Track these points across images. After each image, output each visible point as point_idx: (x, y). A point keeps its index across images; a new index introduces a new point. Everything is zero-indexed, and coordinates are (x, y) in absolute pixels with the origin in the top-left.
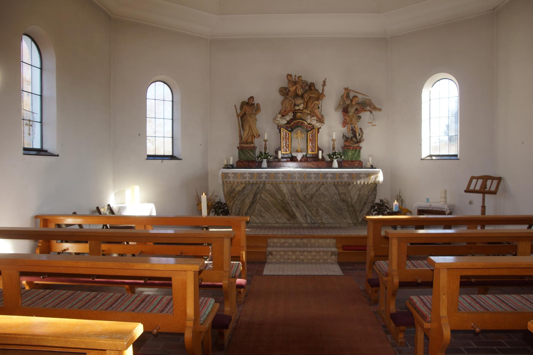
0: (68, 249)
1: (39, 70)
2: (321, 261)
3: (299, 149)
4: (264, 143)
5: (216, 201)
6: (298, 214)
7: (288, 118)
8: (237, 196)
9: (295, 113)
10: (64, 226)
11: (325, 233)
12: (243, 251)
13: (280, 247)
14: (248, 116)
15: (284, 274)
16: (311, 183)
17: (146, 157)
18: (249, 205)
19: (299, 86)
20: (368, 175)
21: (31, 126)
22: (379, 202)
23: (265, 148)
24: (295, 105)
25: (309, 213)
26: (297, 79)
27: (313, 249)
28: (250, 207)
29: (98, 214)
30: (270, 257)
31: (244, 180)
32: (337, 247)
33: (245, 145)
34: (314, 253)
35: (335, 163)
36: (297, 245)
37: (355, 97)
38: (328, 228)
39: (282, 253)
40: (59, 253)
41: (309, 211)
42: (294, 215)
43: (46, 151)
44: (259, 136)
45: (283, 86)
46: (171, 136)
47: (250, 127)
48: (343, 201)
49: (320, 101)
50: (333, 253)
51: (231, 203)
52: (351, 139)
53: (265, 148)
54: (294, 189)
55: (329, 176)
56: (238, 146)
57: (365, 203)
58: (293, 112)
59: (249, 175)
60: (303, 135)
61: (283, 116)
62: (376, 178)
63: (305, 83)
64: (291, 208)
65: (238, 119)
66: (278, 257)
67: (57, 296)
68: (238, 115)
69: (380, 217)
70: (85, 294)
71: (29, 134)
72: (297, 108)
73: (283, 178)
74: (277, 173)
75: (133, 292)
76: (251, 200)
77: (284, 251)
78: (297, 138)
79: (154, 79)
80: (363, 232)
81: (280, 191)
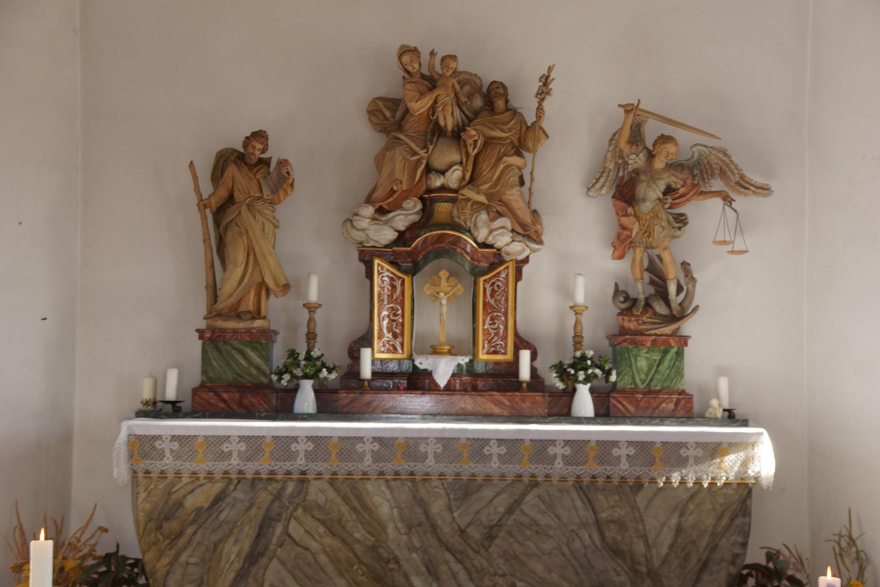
5: (101, 552)
7: (402, 220)
8: (190, 531)
14: (244, 209)
16: (488, 479)
18: (237, 566)
19: (445, 95)
22: (762, 561)
23: (311, 337)
31: (219, 467)
33: (231, 325)
35: (584, 401)
37: (664, 139)
44: (286, 288)
45: (381, 94)
47: (250, 251)
48: (616, 552)
51: (165, 561)
53: (311, 337)
54: (423, 504)
55: (558, 450)
56: (203, 324)
57: (705, 566)
58: (422, 199)
59: (243, 447)
61: (381, 211)
62: (745, 464)
63: (468, 81)
64: (407, 577)
65: (204, 218)
68: (203, 205)
72: (438, 182)
73: (377, 457)
76: (247, 544)
78: (436, 298)
81: (363, 510)
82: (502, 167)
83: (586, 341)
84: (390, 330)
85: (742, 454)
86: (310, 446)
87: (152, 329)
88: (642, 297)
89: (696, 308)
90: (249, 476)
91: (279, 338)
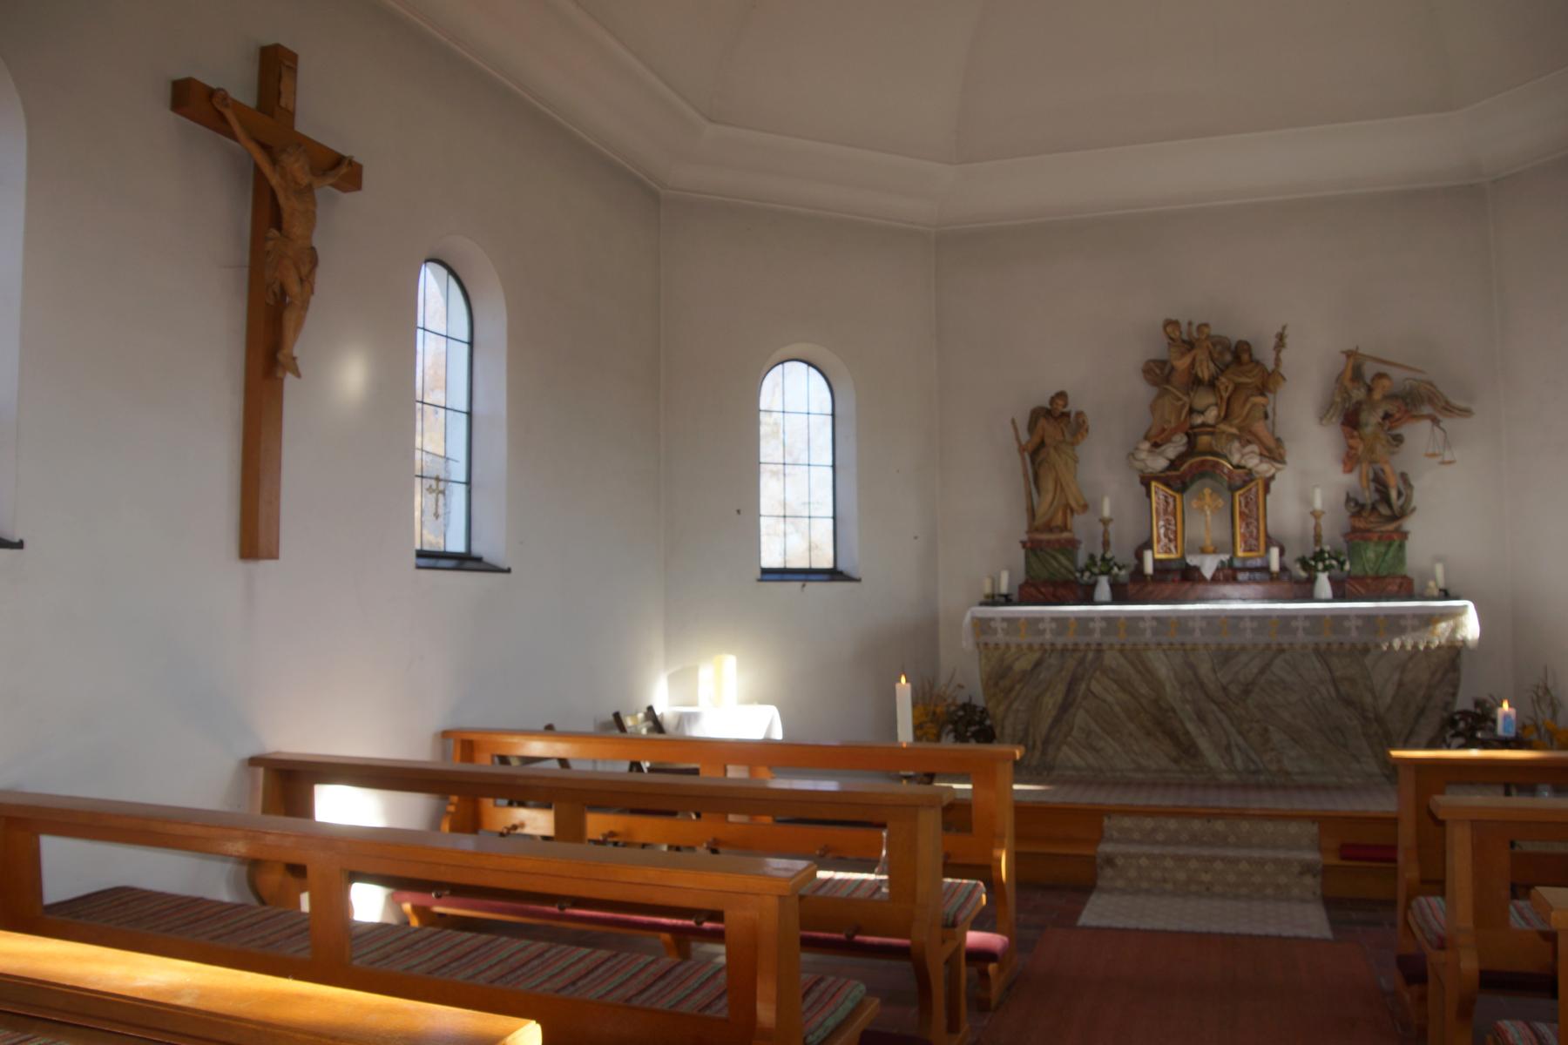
0: (522, 825)
1: (465, 348)
2: (1269, 891)
3: (1208, 542)
4: (1101, 527)
5: (960, 701)
6: (1204, 744)
7: (1172, 451)
8: (1018, 687)
9: (1192, 435)
10: (515, 763)
11: (1282, 803)
12: (1001, 847)
13: (1140, 842)
14: (1052, 451)
15: (1143, 926)
16: (1243, 649)
17: (758, 575)
18: (1054, 713)
19: (1201, 355)
20: (1430, 619)
21: (443, 492)
22: (1470, 707)
23: (1106, 544)
24: (1192, 411)
25: (1240, 740)
26: (1195, 334)
27: (1243, 853)
28: (1057, 721)
29: (617, 732)
30: (1109, 872)
31: (1037, 640)
32: (1321, 850)
33: (1045, 536)
34: (1193, 864)
35: (1323, 584)
36: (1195, 839)
37: (1380, 376)
38: (1299, 788)
39: (1144, 862)
40: (502, 835)
41: (1240, 733)
42: (1193, 745)
43: (479, 560)
44: (1085, 507)
45: (1153, 357)
46: (830, 514)
47: (1057, 482)
48: (1348, 702)
49: (1270, 396)
50: (1307, 869)
51: (1002, 708)
52: (1374, 508)
53: (1106, 544)
54: (1192, 667)
55: (1300, 624)
56: (1025, 537)
57: (1422, 712)
58: (1187, 434)
59: (1054, 625)
60: (1221, 502)
61: (1156, 445)
62: (1454, 630)
63: (1220, 343)
64: (1182, 722)
65: (1023, 459)
66: (1132, 873)
67: (444, 947)
68: (1022, 449)
69: (1474, 753)
70: (518, 944)
71: (437, 516)
72: (1198, 420)
73: (1155, 632)
74: (1182, 621)
75: (685, 954)
76: (1060, 697)
77: (1149, 856)
78: (1202, 510)
79: (778, 356)
80: (1383, 804)
81: (1147, 673)
82: (1248, 406)
83: (1324, 539)
84: (1166, 535)
85: (1451, 623)
86: (1104, 624)
87: (988, 545)
88: (1369, 502)
89: (1414, 510)
90: (1059, 647)
91: (1082, 546)
